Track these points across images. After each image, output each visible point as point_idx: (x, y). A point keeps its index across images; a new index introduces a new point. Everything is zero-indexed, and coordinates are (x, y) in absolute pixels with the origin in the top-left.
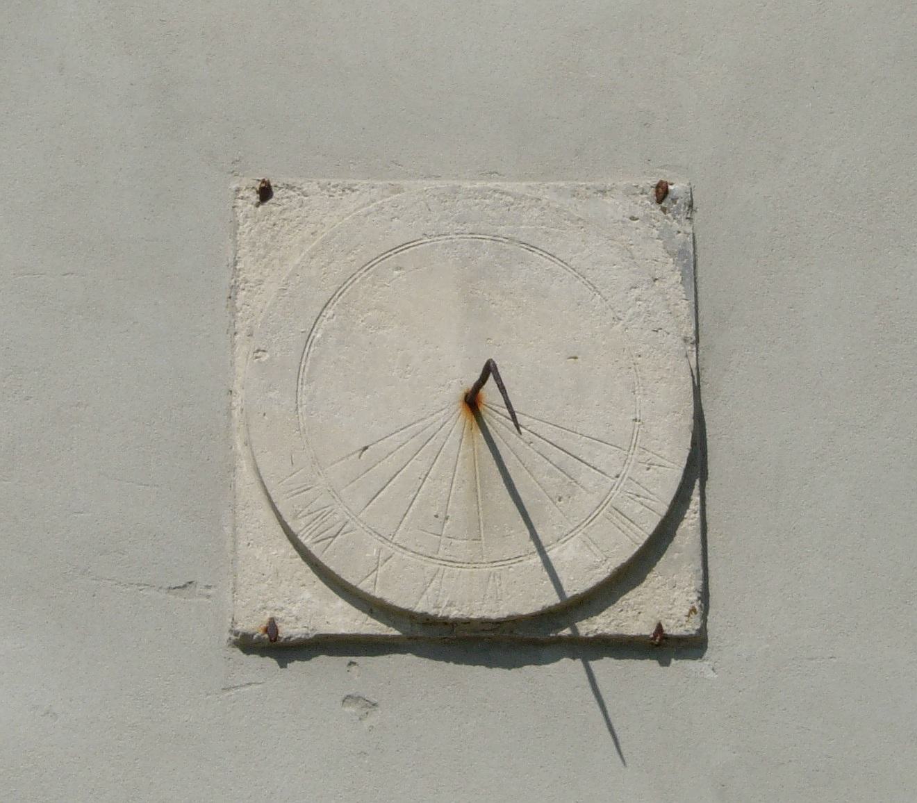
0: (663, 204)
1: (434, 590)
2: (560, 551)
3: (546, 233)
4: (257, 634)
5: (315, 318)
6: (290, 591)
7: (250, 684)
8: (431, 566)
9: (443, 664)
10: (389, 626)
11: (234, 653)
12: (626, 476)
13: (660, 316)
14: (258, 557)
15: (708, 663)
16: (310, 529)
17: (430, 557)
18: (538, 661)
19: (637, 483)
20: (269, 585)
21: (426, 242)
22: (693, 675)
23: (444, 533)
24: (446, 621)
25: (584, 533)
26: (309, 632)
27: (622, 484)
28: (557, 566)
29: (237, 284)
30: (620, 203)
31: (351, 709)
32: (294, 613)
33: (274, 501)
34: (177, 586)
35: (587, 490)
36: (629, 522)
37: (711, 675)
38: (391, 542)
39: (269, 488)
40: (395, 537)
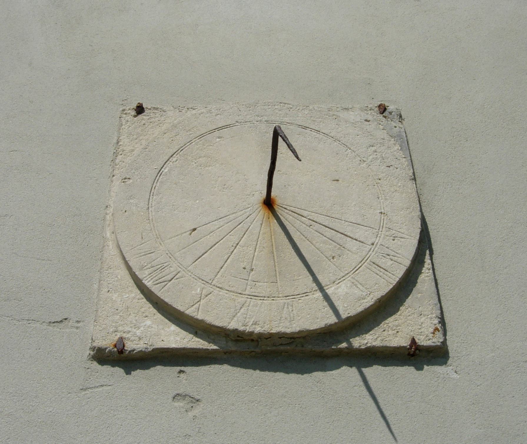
0: (384, 114)
1: (243, 314)
2: (335, 289)
3: (314, 121)
4: (109, 348)
5: (165, 161)
6: (136, 320)
7: (102, 386)
8: (241, 299)
9: (251, 371)
10: (209, 343)
11: (92, 365)
12: (379, 243)
13: (391, 159)
14: (114, 299)
15: (451, 368)
16: (152, 276)
17: (240, 294)
18: (324, 369)
19: (387, 247)
20: (121, 316)
21: (238, 125)
22: (442, 376)
23: (250, 278)
24: (252, 338)
25: (352, 278)
26: (148, 347)
27: (376, 249)
28: (334, 299)
29: (118, 152)
30: (358, 114)
31: (180, 404)
32: (138, 334)
33: (127, 259)
34: (56, 321)
35: (352, 252)
36: (384, 271)
37: (455, 376)
38: (211, 284)
39: (124, 252)
40: (214, 281)
